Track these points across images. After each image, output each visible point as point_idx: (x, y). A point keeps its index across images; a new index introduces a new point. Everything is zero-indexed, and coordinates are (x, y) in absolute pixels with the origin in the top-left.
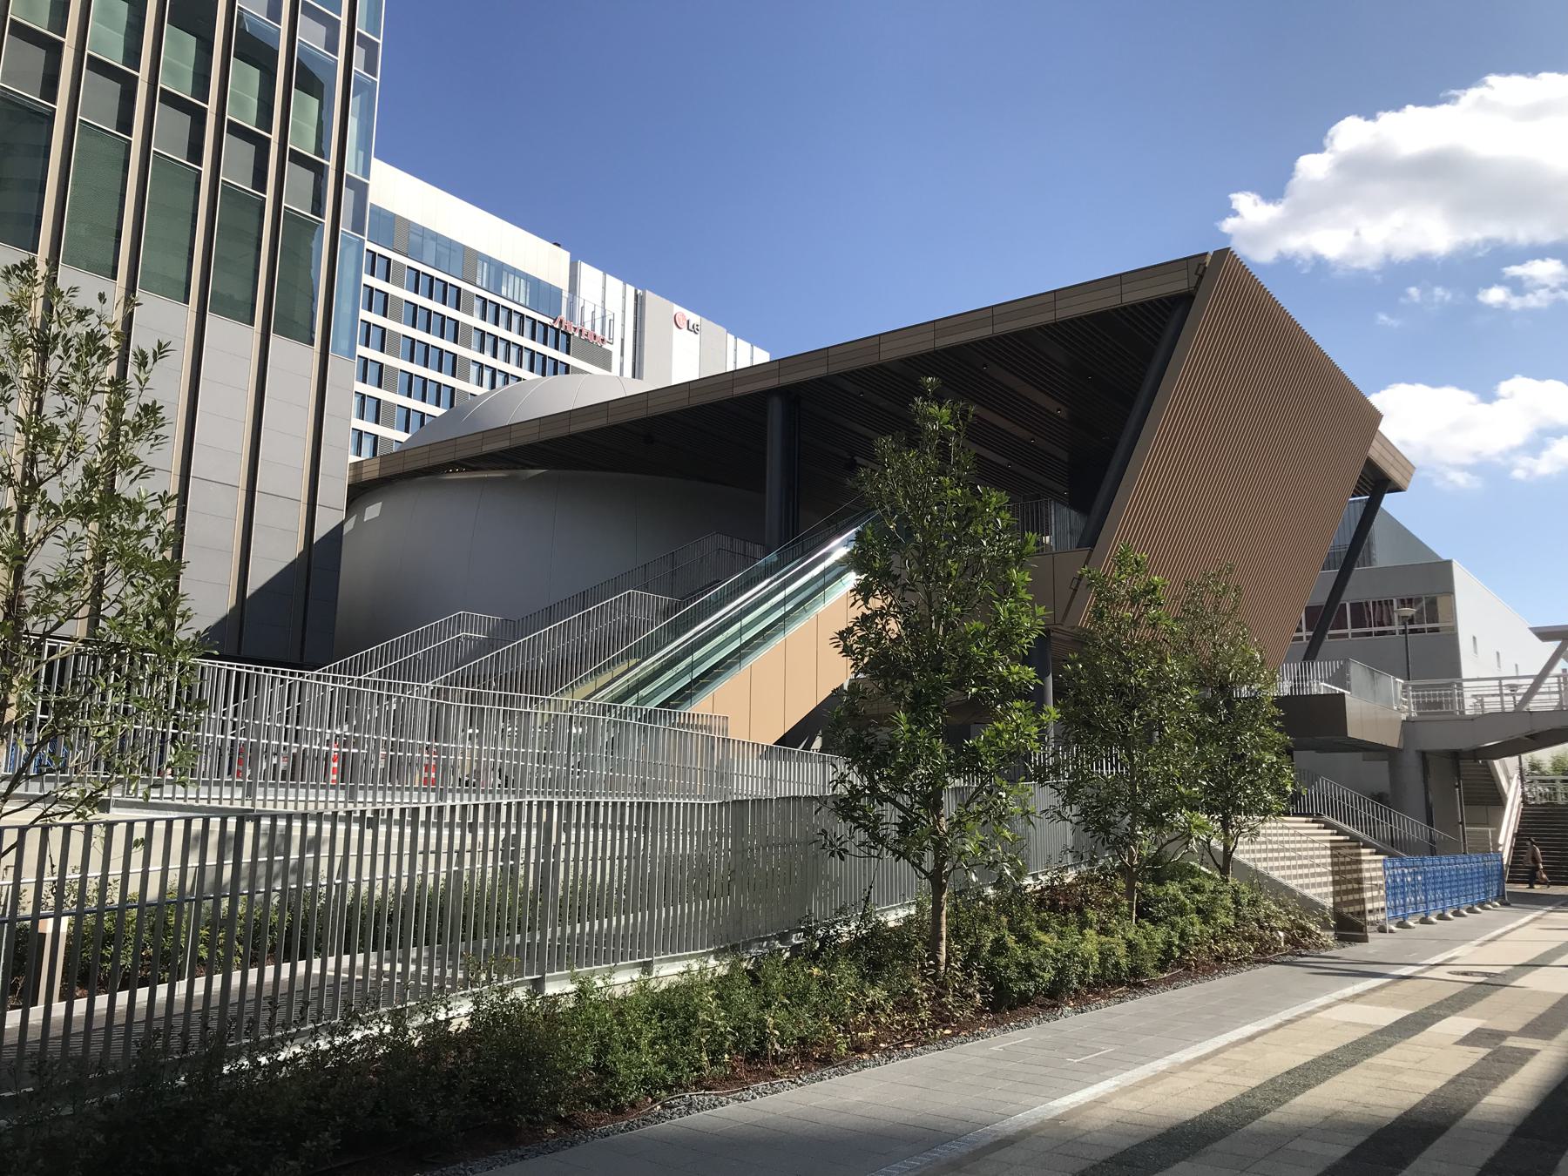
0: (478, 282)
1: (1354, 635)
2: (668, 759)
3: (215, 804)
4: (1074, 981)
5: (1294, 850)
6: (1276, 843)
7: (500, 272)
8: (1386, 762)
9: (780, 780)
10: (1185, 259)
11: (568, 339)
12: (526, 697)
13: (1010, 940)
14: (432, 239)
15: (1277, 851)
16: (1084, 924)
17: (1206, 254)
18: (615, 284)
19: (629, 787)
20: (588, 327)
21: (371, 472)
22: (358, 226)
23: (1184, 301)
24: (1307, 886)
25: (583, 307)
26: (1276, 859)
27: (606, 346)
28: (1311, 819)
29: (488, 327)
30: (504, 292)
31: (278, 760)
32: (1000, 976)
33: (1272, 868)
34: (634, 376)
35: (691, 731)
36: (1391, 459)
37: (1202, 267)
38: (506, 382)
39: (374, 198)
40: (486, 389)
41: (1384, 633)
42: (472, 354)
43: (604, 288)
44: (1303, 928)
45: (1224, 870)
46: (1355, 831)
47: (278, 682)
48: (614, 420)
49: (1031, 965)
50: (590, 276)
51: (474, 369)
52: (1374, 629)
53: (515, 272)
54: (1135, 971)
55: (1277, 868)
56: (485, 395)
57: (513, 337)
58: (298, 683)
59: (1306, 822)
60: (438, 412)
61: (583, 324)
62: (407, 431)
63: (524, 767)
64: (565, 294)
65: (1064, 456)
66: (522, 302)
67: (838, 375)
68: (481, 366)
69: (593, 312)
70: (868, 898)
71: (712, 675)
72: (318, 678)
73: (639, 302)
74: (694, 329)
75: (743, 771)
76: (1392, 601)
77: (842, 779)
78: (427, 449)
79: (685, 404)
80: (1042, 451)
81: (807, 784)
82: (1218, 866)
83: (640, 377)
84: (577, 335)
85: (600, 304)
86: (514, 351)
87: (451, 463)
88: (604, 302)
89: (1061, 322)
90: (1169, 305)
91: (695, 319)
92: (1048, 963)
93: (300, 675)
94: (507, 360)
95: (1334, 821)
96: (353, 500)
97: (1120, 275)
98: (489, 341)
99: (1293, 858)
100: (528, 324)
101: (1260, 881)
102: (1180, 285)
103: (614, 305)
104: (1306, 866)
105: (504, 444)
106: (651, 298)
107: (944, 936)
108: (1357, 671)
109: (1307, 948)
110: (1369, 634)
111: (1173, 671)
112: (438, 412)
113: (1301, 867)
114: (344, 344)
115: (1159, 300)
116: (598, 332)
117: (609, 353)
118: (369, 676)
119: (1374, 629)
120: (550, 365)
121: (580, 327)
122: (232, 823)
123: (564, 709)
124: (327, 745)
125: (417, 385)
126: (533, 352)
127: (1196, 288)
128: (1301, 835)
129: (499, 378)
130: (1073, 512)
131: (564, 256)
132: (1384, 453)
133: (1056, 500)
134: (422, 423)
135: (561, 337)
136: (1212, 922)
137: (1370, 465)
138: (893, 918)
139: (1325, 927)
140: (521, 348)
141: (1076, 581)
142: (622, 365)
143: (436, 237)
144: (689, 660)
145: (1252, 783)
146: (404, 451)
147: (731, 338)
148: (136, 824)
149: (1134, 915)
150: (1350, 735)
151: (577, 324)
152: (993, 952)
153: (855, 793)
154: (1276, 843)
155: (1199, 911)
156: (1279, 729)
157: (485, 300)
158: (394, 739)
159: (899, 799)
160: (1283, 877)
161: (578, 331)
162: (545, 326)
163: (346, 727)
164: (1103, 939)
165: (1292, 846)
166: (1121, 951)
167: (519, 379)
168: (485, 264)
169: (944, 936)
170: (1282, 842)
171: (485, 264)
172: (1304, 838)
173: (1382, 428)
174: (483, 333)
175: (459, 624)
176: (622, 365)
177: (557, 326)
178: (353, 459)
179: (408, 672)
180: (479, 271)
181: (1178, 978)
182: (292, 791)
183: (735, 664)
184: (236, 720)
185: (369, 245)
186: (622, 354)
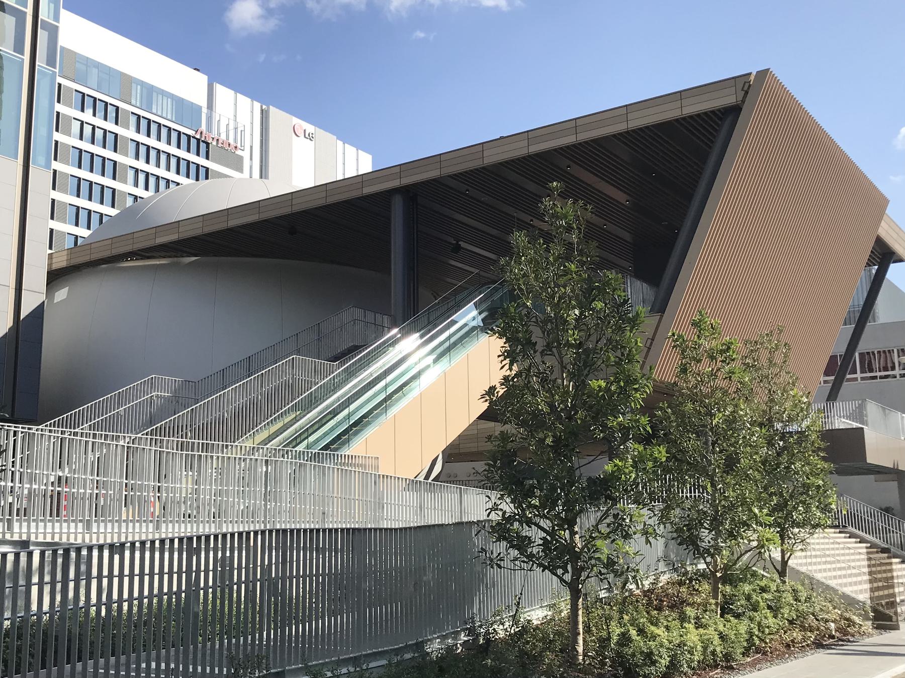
0: (133, 102)
1: (862, 379)
2: (363, 496)
3: (49, 539)
4: (685, 666)
5: (833, 555)
6: (819, 550)
7: (150, 92)
8: (896, 482)
9: (428, 508)
10: (733, 78)
11: (208, 147)
12: (199, 443)
13: (633, 633)
14: (94, 67)
15: (820, 556)
16: (683, 618)
17: (750, 74)
18: (244, 101)
19: (283, 514)
20: (223, 137)
21: (61, 262)
22: (51, 62)
23: (732, 113)
24: (845, 585)
25: (219, 121)
26: (819, 563)
27: (239, 152)
28: (838, 530)
29: (142, 138)
30: (154, 111)
31: (13, 500)
32: (629, 663)
33: (815, 571)
34: (261, 177)
35: (350, 469)
36: (895, 236)
37: (747, 85)
38: (168, 187)
39: (63, 41)
40: (151, 193)
41: (886, 377)
42: (130, 161)
43: (236, 104)
44: (848, 619)
45: (782, 573)
46: (874, 539)
47: (209, 458)
48: (265, 216)
49: (651, 653)
50: (223, 93)
51: (131, 173)
52: (878, 374)
53: (163, 93)
54: (728, 657)
55: (820, 571)
56: (150, 198)
57: (162, 146)
58: (67, 439)
59: (835, 533)
60: (113, 212)
61: (219, 134)
62: (89, 228)
63: (227, 501)
64: (205, 110)
65: (627, 237)
66: (169, 117)
67: (449, 176)
68: (137, 170)
69: (228, 125)
70: (519, 603)
71: (360, 424)
72: (75, 434)
73: (264, 115)
74: (310, 137)
75: (406, 502)
76: (893, 350)
77: (495, 508)
78: (109, 242)
79: (321, 202)
80: (614, 235)
81: (448, 511)
82: (777, 571)
83: (267, 177)
84: (214, 143)
85: (232, 117)
86: (163, 157)
87: (129, 253)
88: (235, 116)
89: (632, 131)
90: (720, 115)
91: (310, 128)
92: (663, 651)
93: (29, 429)
94: (158, 165)
95: (857, 531)
96: (51, 282)
97: (680, 92)
98: (142, 150)
99: (834, 562)
100: (174, 136)
101: (813, 584)
102: (728, 99)
103: (244, 119)
104: (844, 568)
105: (174, 237)
106: (273, 110)
107: (581, 631)
108: (872, 409)
109: (853, 636)
110: (875, 378)
111: (746, 414)
112: (113, 212)
113: (840, 569)
114: (41, 160)
115: (713, 112)
116: (231, 141)
117: (241, 158)
118: (82, 429)
119: (878, 374)
120: (202, 172)
121: (216, 137)
122: (84, 552)
123: (306, 458)
124: (52, 486)
125: (84, 187)
126: (179, 159)
127: (743, 101)
128: (850, 548)
129: (162, 184)
130: (644, 284)
131: (201, 79)
132: (891, 232)
133: (631, 276)
134: (101, 222)
135: (202, 145)
136: (780, 616)
137: (879, 242)
138: (536, 615)
139: (866, 618)
140: (169, 155)
141: (649, 341)
142: (251, 167)
143: (98, 65)
144: (345, 412)
145: (803, 503)
146: (89, 245)
147: (340, 143)
148: (8, 555)
149: (719, 612)
150: (869, 461)
151: (214, 134)
152: (620, 644)
153: (509, 520)
154: (819, 550)
155: (769, 607)
156: (824, 459)
157: (139, 117)
158: (133, 482)
159: (542, 524)
160: (825, 578)
161: (215, 140)
162: (189, 137)
163: (67, 470)
164: (701, 631)
165: (832, 552)
166: (717, 641)
167: (178, 184)
168: (169, 100)
169: (581, 631)
170: (823, 549)
171: (169, 100)
172: (852, 551)
173: (888, 211)
174: (138, 143)
175: (152, 384)
176: (251, 167)
177: (198, 136)
178: (50, 252)
179: (110, 425)
180: (133, 93)
181: (758, 661)
182: (102, 525)
183: (382, 414)
184: (21, 470)
185: (59, 80)
186: (251, 159)
